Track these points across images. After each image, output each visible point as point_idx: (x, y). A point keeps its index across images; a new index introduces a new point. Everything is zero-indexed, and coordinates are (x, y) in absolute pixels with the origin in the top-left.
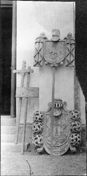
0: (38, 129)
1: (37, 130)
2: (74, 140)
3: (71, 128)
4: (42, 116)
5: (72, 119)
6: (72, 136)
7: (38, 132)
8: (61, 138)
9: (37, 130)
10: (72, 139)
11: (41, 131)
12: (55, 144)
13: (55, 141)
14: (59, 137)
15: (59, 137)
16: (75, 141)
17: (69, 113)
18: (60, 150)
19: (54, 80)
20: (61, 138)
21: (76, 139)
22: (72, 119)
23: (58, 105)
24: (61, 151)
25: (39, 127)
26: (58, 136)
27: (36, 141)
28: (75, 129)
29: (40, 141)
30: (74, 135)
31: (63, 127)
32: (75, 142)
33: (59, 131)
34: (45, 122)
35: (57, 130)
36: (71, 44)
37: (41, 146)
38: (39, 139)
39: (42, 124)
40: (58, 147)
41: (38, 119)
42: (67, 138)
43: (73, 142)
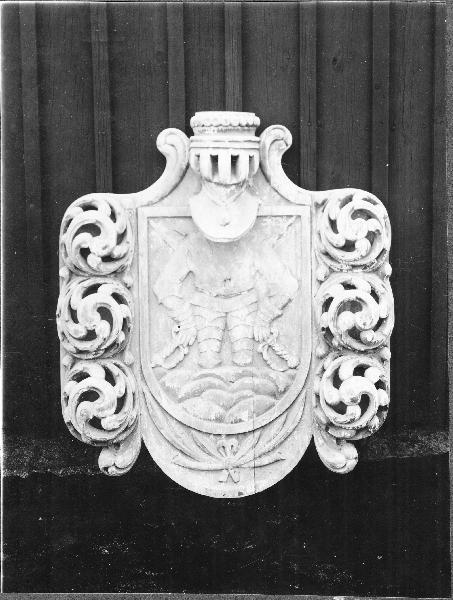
0: (102, 328)
1: (91, 335)
2: (350, 410)
3: (326, 320)
4: (121, 237)
5: (327, 254)
6: (337, 381)
7: (98, 349)
8: (257, 381)
9: (91, 335)
10: (333, 395)
11: (122, 337)
12: (219, 420)
13: (217, 400)
14: (241, 376)
15: (241, 376)
16: (354, 410)
17: (305, 212)
18: (250, 455)
19: (176, 186)
20: (257, 381)
21: (364, 402)
22: (327, 254)
23: (234, 159)
24: (258, 463)
25: (105, 313)
26: (234, 364)
27: (90, 408)
28: (355, 333)
29: (117, 412)
30: (348, 364)
31: (271, 307)
32: (353, 421)
33: (239, 333)
34: (144, 271)
35: (226, 328)
36: (234, 353)
37: (125, 435)
38: (109, 393)
39: (122, 291)
40: (234, 441)
41: (94, 260)
42: (293, 378)
43: (341, 418)
